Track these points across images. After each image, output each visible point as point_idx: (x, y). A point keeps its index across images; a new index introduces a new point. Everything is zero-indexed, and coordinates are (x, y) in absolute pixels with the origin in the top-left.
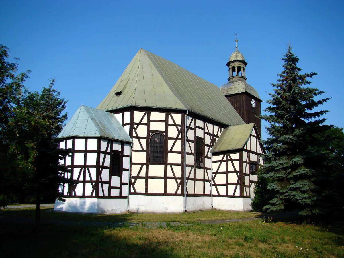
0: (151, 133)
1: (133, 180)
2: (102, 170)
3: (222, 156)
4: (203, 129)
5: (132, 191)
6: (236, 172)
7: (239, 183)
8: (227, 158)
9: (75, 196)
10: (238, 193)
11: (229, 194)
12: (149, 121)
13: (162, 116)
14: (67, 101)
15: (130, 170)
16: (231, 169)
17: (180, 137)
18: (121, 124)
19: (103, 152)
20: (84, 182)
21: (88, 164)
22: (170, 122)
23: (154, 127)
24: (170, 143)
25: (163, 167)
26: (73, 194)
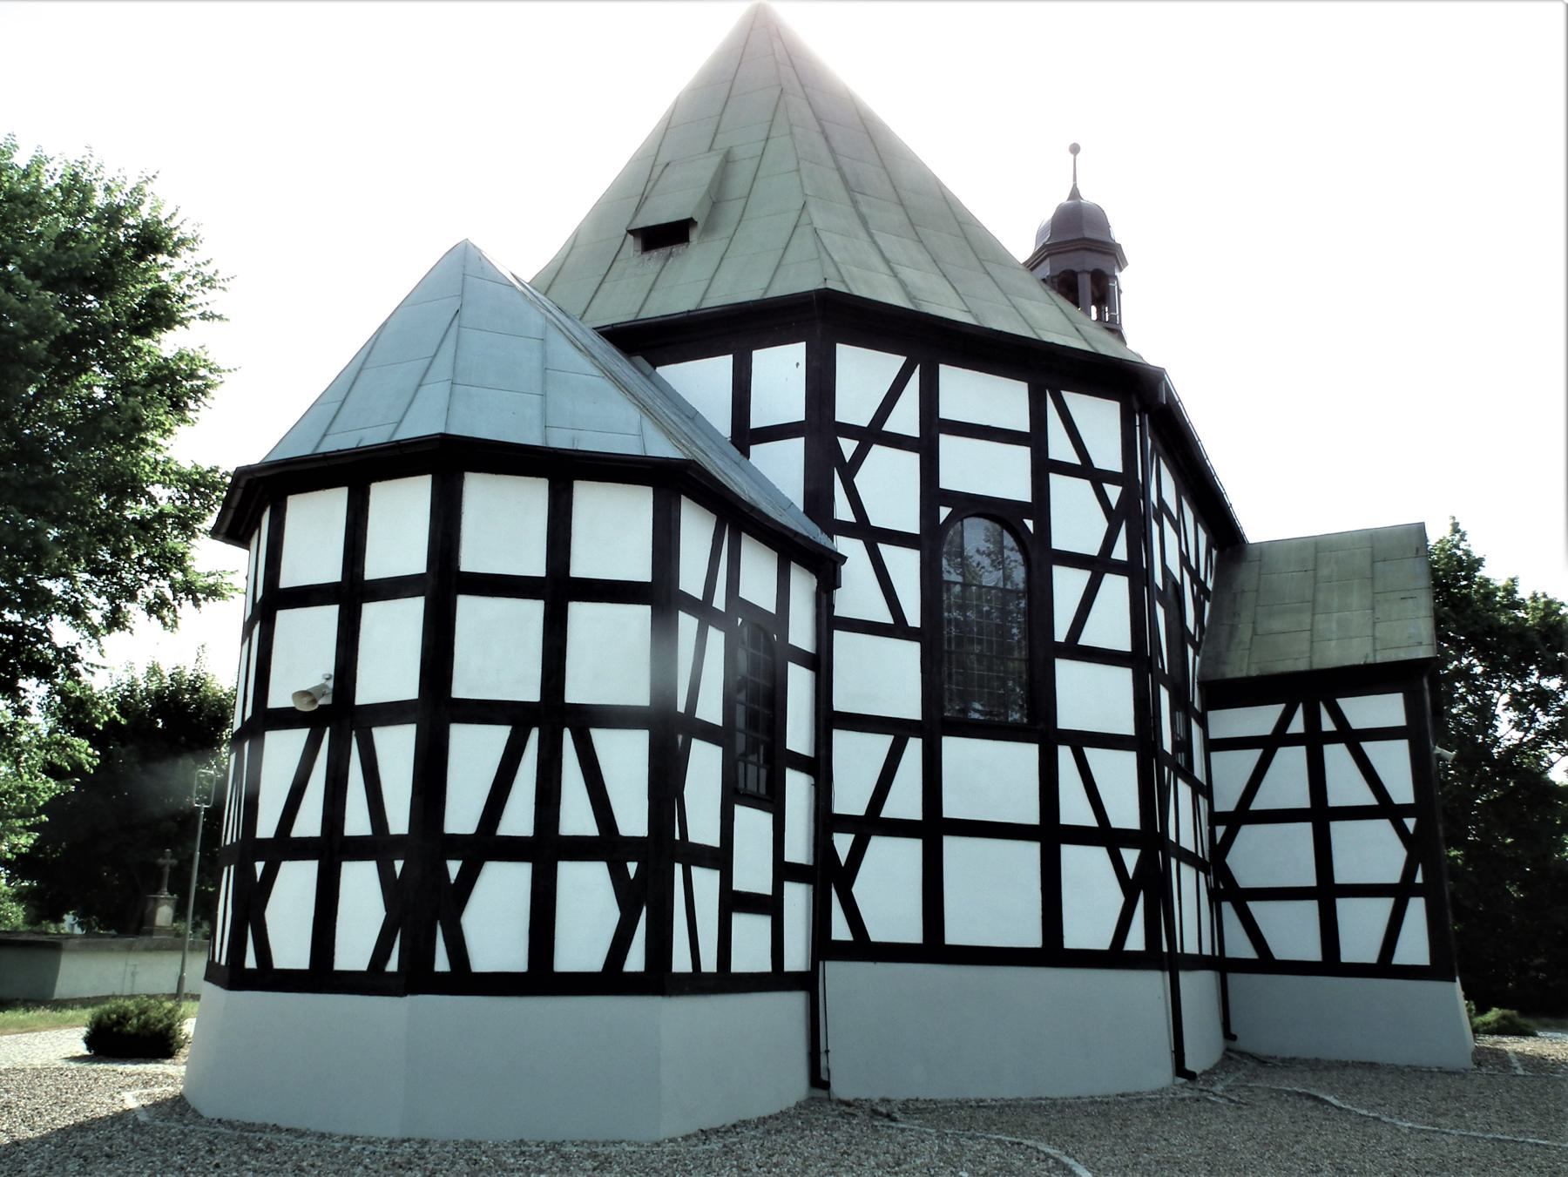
0: (944, 512)
1: (843, 843)
3: (1276, 710)
5: (840, 930)
6: (1385, 808)
7: (1419, 879)
8: (1312, 720)
9: (464, 981)
11: (1348, 955)
12: (933, 425)
14: (220, 317)
15: (819, 767)
16: (1346, 786)
17: (1120, 552)
18: (724, 427)
20: (546, 851)
21: (576, 693)
22: (1060, 448)
23: (973, 469)
24: (1068, 585)
25: (1028, 754)
26: (442, 963)
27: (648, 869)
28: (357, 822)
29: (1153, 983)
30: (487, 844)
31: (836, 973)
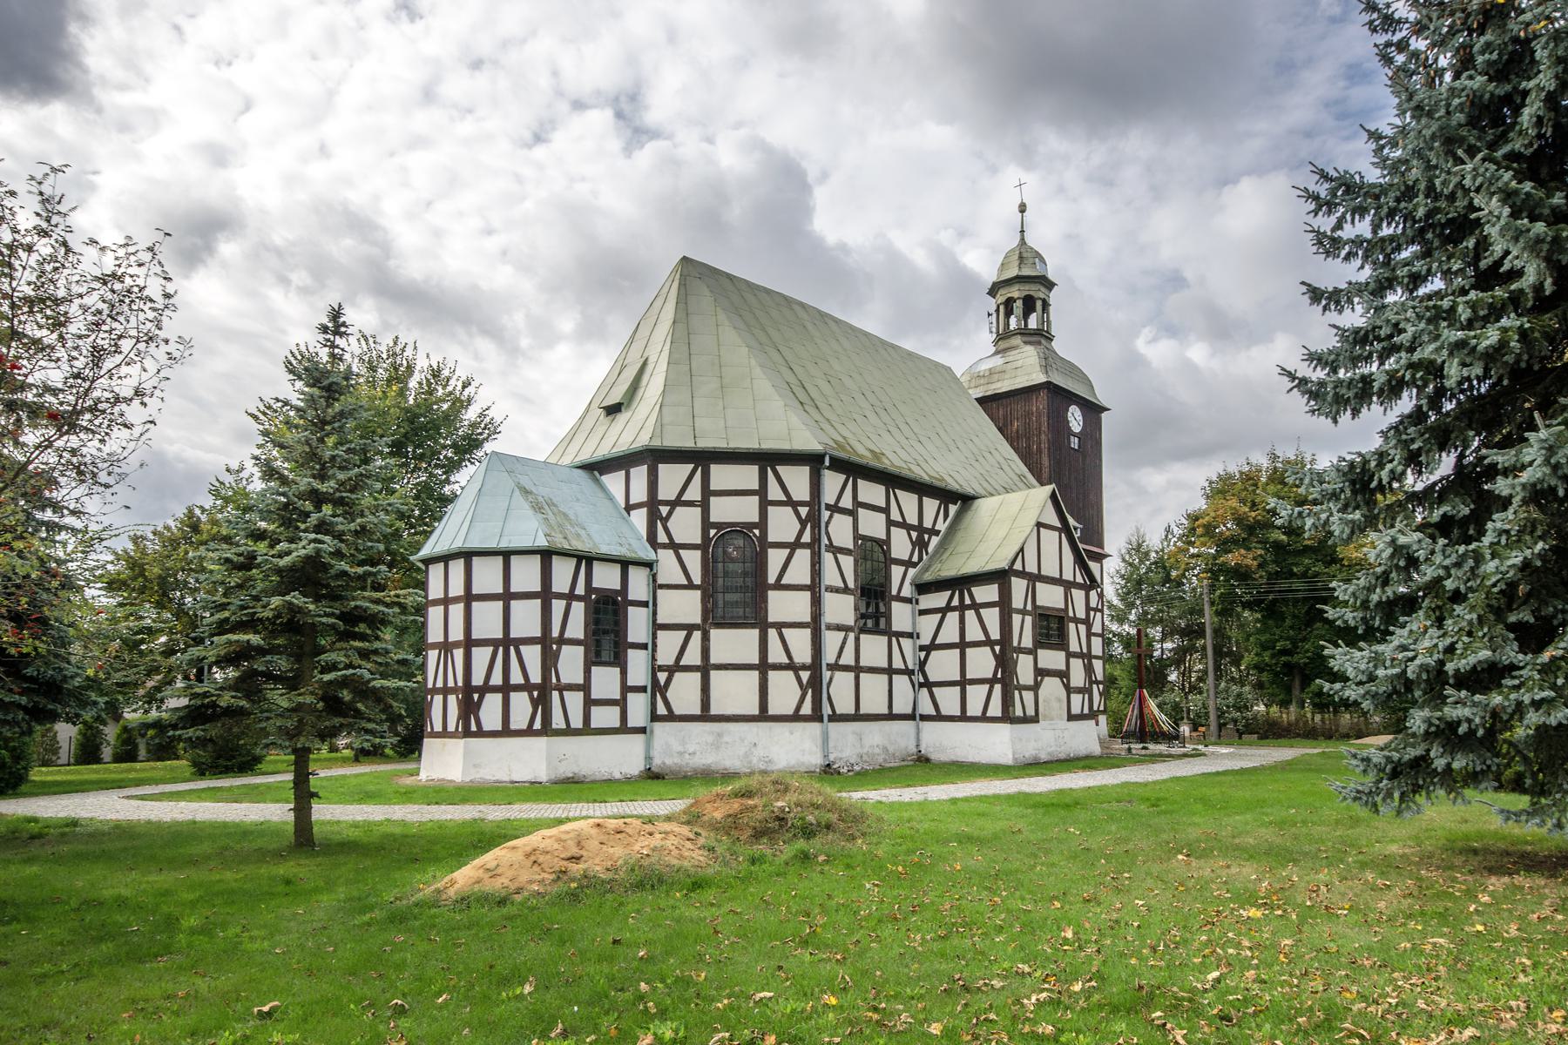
1: (662, 677)
2: (559, 650)
4: (886, 510)
9: (481, 733)
10: (995, 709)
11: (513, 727)
12: (707, 493)
13: (746, 476)
15: (651, 647)
16: (974, 633)
17: (806, 538)
19: (560, 596)
20: (506, 689)
22: (775, 492)
23: (723, 511)
24: (775, 558)
26: (474, 728)
27: (542, 695)
28: (451, 684)
29: (815, 727)
30: (486, 689)
31: (658, 727)
